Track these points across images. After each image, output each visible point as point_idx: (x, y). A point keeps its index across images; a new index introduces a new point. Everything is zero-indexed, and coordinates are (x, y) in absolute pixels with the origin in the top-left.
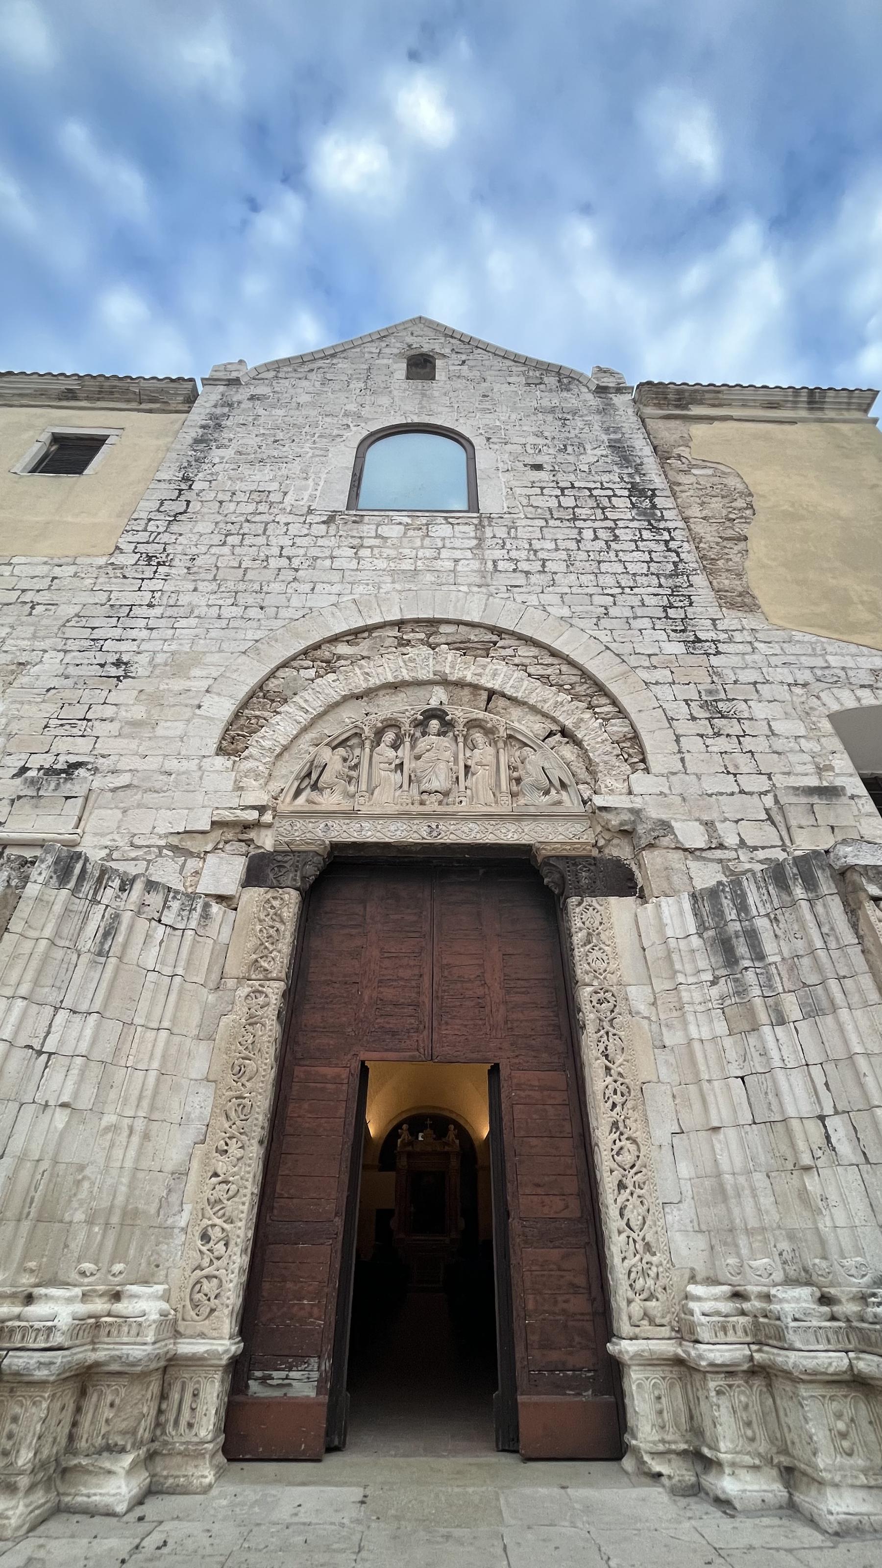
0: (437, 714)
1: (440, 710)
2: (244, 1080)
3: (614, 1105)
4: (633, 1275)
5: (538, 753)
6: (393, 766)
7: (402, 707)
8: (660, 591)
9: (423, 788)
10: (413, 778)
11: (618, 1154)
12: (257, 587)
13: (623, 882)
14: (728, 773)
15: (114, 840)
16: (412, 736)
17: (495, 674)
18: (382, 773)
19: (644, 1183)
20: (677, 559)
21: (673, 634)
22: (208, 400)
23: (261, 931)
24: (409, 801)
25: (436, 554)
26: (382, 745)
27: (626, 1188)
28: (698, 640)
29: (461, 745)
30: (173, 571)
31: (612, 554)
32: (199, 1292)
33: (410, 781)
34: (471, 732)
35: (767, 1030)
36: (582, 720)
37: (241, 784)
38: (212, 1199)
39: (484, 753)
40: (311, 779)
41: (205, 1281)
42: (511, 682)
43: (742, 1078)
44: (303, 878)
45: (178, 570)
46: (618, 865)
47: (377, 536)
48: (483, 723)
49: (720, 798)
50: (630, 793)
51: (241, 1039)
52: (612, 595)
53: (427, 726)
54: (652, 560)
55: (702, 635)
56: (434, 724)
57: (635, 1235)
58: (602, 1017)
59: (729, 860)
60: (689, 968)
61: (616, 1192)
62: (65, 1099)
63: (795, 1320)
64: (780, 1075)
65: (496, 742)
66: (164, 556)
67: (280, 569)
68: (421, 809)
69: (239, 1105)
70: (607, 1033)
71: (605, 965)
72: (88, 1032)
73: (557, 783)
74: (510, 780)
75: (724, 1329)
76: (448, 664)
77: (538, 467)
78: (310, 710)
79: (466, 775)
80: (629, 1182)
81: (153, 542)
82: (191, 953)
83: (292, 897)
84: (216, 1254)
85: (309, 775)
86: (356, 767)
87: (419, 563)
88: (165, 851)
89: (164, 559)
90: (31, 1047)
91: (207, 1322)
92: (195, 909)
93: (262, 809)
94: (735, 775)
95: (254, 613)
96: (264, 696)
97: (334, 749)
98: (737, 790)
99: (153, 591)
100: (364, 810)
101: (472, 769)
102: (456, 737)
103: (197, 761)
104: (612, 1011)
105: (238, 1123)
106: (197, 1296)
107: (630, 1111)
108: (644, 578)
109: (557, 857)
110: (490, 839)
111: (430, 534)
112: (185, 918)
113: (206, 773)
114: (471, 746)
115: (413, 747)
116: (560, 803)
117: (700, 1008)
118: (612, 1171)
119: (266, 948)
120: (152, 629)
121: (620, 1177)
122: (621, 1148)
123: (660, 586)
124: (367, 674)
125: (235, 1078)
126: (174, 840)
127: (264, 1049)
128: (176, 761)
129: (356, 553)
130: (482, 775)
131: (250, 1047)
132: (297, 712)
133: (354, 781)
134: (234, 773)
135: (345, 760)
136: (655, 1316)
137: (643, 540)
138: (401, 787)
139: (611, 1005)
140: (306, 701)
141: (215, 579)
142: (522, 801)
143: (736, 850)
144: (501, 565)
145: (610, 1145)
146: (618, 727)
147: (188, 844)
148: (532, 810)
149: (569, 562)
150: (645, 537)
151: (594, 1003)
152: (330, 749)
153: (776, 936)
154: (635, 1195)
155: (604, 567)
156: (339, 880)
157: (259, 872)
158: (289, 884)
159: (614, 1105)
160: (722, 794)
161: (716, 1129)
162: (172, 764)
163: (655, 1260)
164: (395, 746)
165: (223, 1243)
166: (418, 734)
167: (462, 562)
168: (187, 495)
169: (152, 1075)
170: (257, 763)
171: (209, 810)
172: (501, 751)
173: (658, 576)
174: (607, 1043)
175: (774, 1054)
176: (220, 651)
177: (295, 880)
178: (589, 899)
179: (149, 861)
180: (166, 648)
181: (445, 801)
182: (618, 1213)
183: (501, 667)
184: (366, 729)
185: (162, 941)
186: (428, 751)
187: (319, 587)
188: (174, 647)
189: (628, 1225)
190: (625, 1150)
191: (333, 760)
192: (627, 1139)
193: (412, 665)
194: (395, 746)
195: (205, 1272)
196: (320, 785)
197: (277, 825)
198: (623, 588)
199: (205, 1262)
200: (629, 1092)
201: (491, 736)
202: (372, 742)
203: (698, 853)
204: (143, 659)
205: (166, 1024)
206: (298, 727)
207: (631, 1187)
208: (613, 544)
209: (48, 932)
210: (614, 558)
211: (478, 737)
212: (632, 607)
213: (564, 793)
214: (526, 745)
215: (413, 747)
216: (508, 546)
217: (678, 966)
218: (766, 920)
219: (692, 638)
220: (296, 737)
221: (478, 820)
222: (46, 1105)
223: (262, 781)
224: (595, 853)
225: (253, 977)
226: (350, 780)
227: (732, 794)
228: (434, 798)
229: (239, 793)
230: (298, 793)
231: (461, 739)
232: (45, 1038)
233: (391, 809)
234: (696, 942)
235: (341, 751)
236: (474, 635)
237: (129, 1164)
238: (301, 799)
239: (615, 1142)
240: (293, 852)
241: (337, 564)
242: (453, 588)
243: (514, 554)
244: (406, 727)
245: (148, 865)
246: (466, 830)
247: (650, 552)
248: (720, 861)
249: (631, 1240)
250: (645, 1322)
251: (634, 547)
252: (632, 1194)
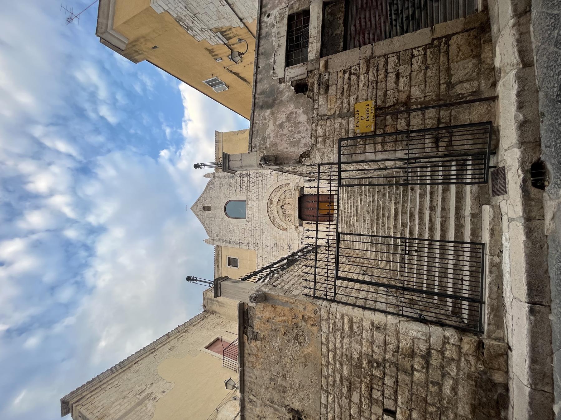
0: (281, 207)
7: (280, 211)
13: (302, 188)
17: (275, 200)
22: (218, 243)
39: (287, 202)
40: (290, 221)
77: (235, 191)
96: (279, 227)
146: (284, 186)
149: (256, 188)
156: (301, 217)
157: (301, 225)
168: (243, 242)
183: (274, 199)
191: (287, 219)
236: (269, 202)
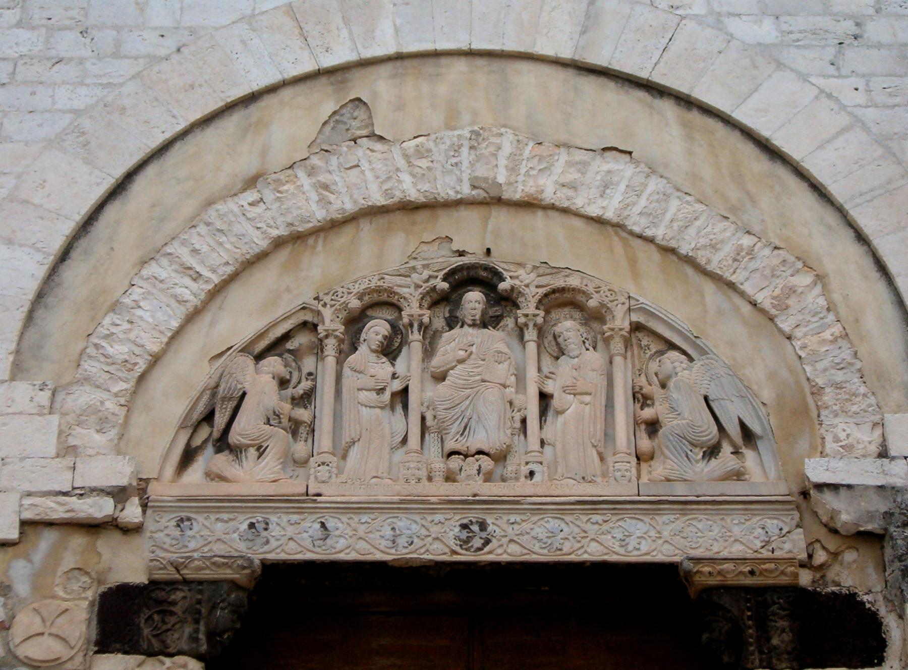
1: (486, 268)
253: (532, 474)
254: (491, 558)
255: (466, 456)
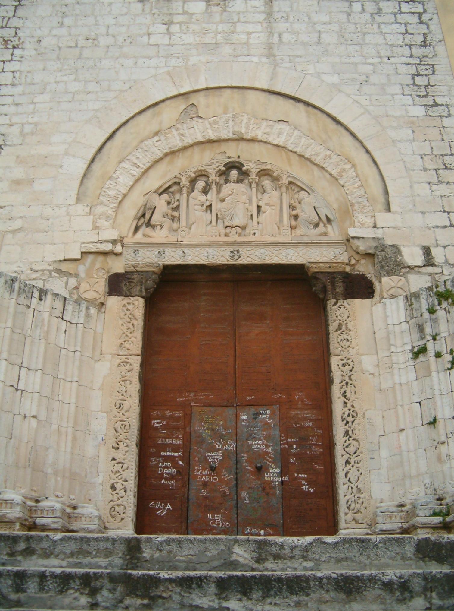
1: (238, 162)
2: (123, 411)
3: (347, 422)
4: (349, 503)
5: (311, 196)
6: (204, 207)
8: (411, 61)
9: (227, 224)
10: (219, 216)
11: (347, 447)
12: (91, 63)
14: (445, 211)
15: (19, 267)
16: (217, 183)
18: (197, 212)
19: (360, 461)
20: (426, 31)
21: (417, 99)
23: (122, 325)
24: (217, 234)
25: (232, 29)
26: (196, 191)
27: (350, 463)
28: (436, 105)
29: (254, 190)
30: (26, 53)
31: (375, 26)
32: (114, 511)
33: (217, 218)
34: (262, 179)
35: (434, 374)
36: (344, 170)
37: (97, 224)
38: (114, 471)
39: (272, 196)
40: (145, 219)
41: (116, 506)
42: (292, 139)
43: (420, 403)
44: (146, 290)
45: (29, 51)
46: (362, 278)
47: (185, 13)
48: (271, 173)
49: (436, 230)
50: (375, 227)
51: (118, 389)
52: (372, 64)
53: (228, 175)
54: (407, 32)
55: (439, 100)
56: (234, 173)
57: (352, 486)
58: (344, 374)
59: (436, 274)
60: (399, 343)
61: (344, 465)
62: (34, 413)
63: (422, 505)
64: (438, 398)
65: (280, 187)
66: (16, 39)
67: (108, 47)
68: (226, 239)
69: (122, 425)
70: (347, 383)
71: (349, 343)
72: (38, 380)
73: (324, 218)
74: (291, 216)
75: (391, 517)
76: (243, 125)
78: (141, 166)
79: (258, 212)
80: (352, 461)
81: (6, 27)
82: (83, 338)
83: (140, 302)
84: (120, 495)
85: (144, 215)
86: (177, 208)
87: (219, 37)
88: (53, 274)
89: (17, 42)
90: (12, 386)
91: (120, 523)
92: (81, 311)
93: (114, 242)
94: (449, 213)
95: (92, 87)
97: (160, 194)
98: (448, 224)
99: (13, 72)
100: (186, 241)
101: (262, 209)
102: (250, 184)
103: (65, 209)
104: (351, 371)
105: (123, 434)
106: (113, 513)
107: (357, 425)
108: (400, 49)
109: (322, 272)
110: (275, 260)
111: (228, 9)
112: (77, 317)
113: (73, 218)
114: (262, 191)
115: (219, 192)
116: (325, 234)
117: (402, 366)
118: (342, 456)
119: (127, 336)
120: (17, 105)
121: (347, 458)
122: (349, 445)
123: (411, 56)
124: (182, 135)
125: (118, 410)
126: (57, 266)
127: (133, 395)
128: (51, 209)
129: (168, 29)
130: (269, 213)
131: (125, 394)
132: (132, 168)
133: (176, 219)
134: (91, 217)
135: (169, 203)
136: (359, 520)
137: (401, 13)
138: (211, 223)
139: (350, 368)
140: (137, 158)
141: (58, 58)
142: (298, 232)
143: (442, 267)
144: (286, 37)
145: (343, 443)
147: (64, 267)
148: (306, 239)
150: (403, 10)
151: (340, 366)
152: (157, 196)
153: (448, 321)
154: (354, 467)
155: (368, 38)
156: (168, 291)
158: (137, 293)
159: (347, 422)
160: (437, 227)
161: (402, 430)
162: (48, 211)
163: (362, 496)
164: (205, 191)
165: (123, 490)
166: (222, 182)
167: (253, 35)
169: (73, 406)
170: (106, 208)
171: (79, 244)
172: (284, 194)
173: (410, 46)
174: (346, 388)
175: (436, 387)
176: (70, 120)
177: (141, 291)
178: (342, 301)
179: (44, 280)
180: (30, 120)
181: (243, 234)
182: (344, 475)
184: (183, 179)
185: (65, 331)
186: (230, 195)
187: (141, 61)
188: (35, 120)
189: (349, 481)
190: (352, 445)
192: (353, 440)
193: (216, 126)
194: (205, 191)
195: (116, 503)
196: (152, 222)
197: (125, 253)
198: (381, 57)
199: (115, 498)
200: (357, 415)
201: (276, 182)
202: (188, 188)
203: (416, 269)
204: (15, 130)
205: (76, 379)
206: (133, 179)
207: (352, 463)
208: (376, 17)
209: (9, 324)
210: (376, 30)
211: (267, 183)
212: (388, 75)
213: (329, 226)
214: (303, 189)
215: (219, 192)
216: (291, 19)
217: (392, 342)
218: (444, 311)
219: (431, 103)
220: (132, 187)
221: (270, 243)
222: (25, 417)
223: (111, 221)
224: (348, 269)
225: (121, 353)
226: (173, 218)
227: (445, 227)
228: (234, 231)
229: (97, 231)
230: (137, 229)
231: (254, 185)
232: (18, 381)
233: (205, 240)
234: (405, 326)
235: (165, 196)
237: (69, 449)
238: (139, 235)
239: (345, 442)
240: (137, 272)
241: (153, 40)
242: (247, 59)
243: (297, 26)
244: (213, 177)
245: (44, 283)
246: (257, 253)
247: (406, 24)
248: (430, 275)
249: (350, 487)
250: (354, 522)
251: (393, 20)
252: (353, 466)
253: (255, 233)
254: (241, 262)
255: (232, 228)
